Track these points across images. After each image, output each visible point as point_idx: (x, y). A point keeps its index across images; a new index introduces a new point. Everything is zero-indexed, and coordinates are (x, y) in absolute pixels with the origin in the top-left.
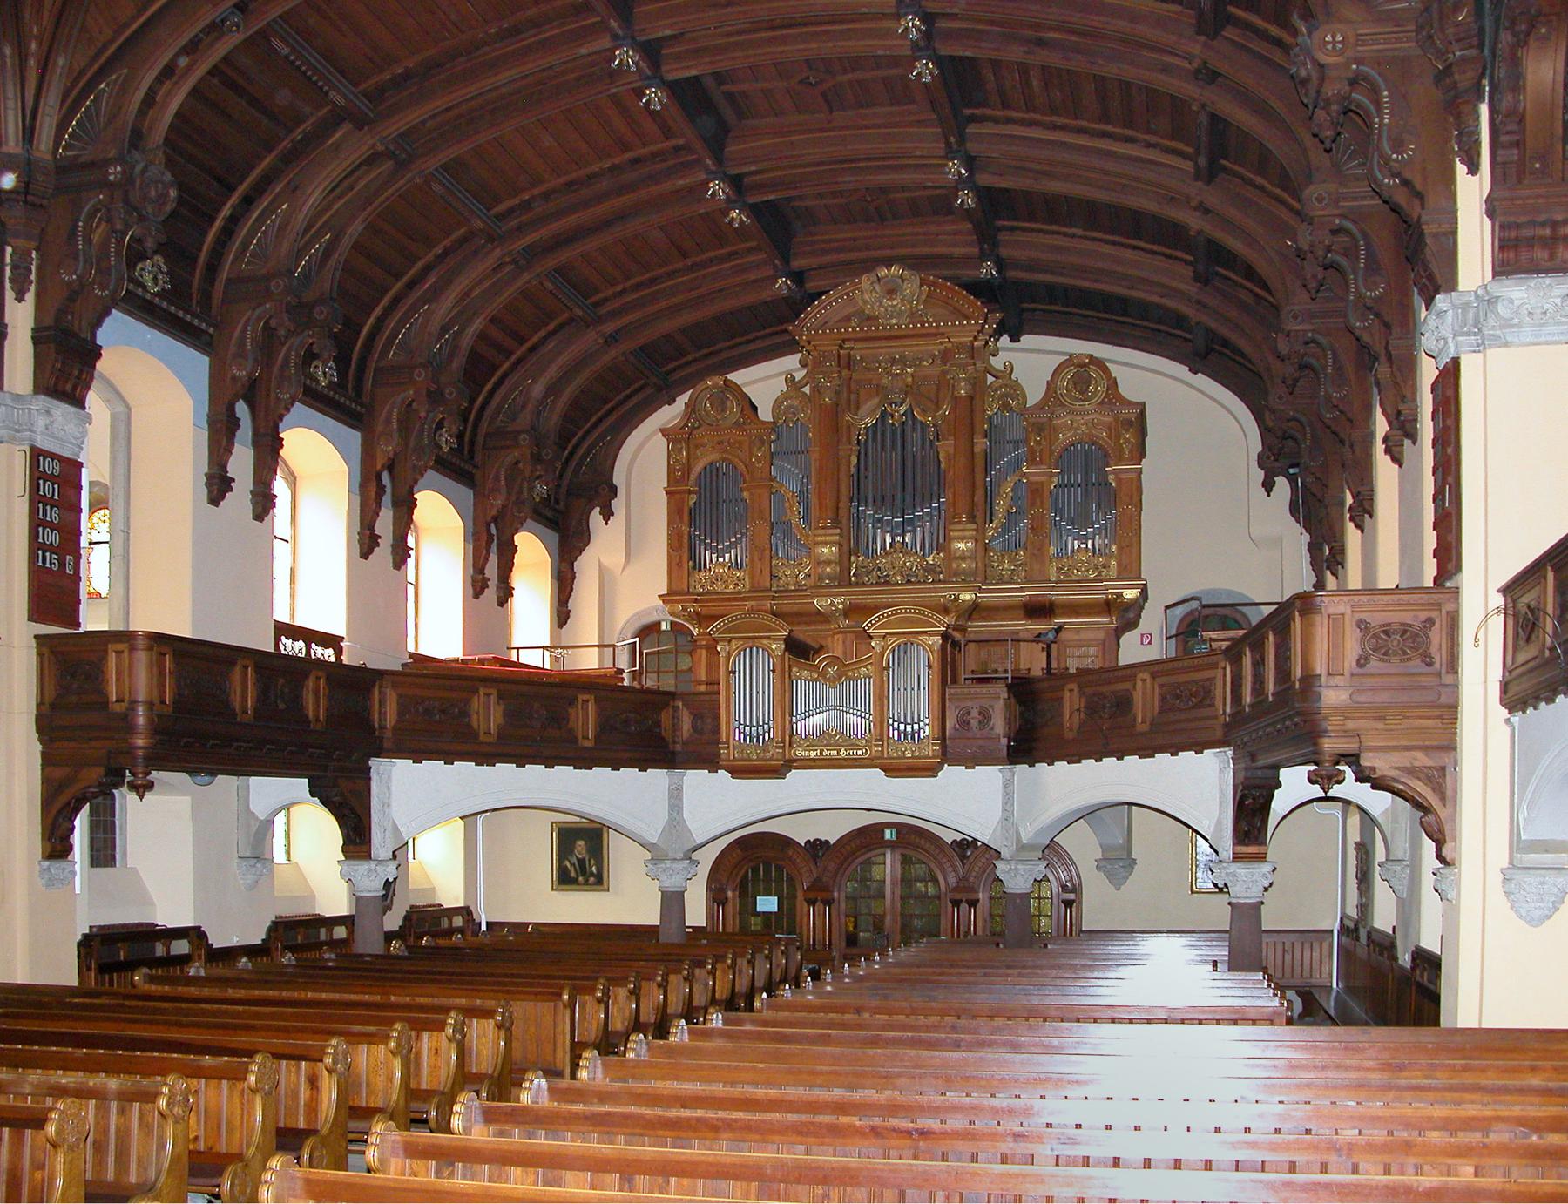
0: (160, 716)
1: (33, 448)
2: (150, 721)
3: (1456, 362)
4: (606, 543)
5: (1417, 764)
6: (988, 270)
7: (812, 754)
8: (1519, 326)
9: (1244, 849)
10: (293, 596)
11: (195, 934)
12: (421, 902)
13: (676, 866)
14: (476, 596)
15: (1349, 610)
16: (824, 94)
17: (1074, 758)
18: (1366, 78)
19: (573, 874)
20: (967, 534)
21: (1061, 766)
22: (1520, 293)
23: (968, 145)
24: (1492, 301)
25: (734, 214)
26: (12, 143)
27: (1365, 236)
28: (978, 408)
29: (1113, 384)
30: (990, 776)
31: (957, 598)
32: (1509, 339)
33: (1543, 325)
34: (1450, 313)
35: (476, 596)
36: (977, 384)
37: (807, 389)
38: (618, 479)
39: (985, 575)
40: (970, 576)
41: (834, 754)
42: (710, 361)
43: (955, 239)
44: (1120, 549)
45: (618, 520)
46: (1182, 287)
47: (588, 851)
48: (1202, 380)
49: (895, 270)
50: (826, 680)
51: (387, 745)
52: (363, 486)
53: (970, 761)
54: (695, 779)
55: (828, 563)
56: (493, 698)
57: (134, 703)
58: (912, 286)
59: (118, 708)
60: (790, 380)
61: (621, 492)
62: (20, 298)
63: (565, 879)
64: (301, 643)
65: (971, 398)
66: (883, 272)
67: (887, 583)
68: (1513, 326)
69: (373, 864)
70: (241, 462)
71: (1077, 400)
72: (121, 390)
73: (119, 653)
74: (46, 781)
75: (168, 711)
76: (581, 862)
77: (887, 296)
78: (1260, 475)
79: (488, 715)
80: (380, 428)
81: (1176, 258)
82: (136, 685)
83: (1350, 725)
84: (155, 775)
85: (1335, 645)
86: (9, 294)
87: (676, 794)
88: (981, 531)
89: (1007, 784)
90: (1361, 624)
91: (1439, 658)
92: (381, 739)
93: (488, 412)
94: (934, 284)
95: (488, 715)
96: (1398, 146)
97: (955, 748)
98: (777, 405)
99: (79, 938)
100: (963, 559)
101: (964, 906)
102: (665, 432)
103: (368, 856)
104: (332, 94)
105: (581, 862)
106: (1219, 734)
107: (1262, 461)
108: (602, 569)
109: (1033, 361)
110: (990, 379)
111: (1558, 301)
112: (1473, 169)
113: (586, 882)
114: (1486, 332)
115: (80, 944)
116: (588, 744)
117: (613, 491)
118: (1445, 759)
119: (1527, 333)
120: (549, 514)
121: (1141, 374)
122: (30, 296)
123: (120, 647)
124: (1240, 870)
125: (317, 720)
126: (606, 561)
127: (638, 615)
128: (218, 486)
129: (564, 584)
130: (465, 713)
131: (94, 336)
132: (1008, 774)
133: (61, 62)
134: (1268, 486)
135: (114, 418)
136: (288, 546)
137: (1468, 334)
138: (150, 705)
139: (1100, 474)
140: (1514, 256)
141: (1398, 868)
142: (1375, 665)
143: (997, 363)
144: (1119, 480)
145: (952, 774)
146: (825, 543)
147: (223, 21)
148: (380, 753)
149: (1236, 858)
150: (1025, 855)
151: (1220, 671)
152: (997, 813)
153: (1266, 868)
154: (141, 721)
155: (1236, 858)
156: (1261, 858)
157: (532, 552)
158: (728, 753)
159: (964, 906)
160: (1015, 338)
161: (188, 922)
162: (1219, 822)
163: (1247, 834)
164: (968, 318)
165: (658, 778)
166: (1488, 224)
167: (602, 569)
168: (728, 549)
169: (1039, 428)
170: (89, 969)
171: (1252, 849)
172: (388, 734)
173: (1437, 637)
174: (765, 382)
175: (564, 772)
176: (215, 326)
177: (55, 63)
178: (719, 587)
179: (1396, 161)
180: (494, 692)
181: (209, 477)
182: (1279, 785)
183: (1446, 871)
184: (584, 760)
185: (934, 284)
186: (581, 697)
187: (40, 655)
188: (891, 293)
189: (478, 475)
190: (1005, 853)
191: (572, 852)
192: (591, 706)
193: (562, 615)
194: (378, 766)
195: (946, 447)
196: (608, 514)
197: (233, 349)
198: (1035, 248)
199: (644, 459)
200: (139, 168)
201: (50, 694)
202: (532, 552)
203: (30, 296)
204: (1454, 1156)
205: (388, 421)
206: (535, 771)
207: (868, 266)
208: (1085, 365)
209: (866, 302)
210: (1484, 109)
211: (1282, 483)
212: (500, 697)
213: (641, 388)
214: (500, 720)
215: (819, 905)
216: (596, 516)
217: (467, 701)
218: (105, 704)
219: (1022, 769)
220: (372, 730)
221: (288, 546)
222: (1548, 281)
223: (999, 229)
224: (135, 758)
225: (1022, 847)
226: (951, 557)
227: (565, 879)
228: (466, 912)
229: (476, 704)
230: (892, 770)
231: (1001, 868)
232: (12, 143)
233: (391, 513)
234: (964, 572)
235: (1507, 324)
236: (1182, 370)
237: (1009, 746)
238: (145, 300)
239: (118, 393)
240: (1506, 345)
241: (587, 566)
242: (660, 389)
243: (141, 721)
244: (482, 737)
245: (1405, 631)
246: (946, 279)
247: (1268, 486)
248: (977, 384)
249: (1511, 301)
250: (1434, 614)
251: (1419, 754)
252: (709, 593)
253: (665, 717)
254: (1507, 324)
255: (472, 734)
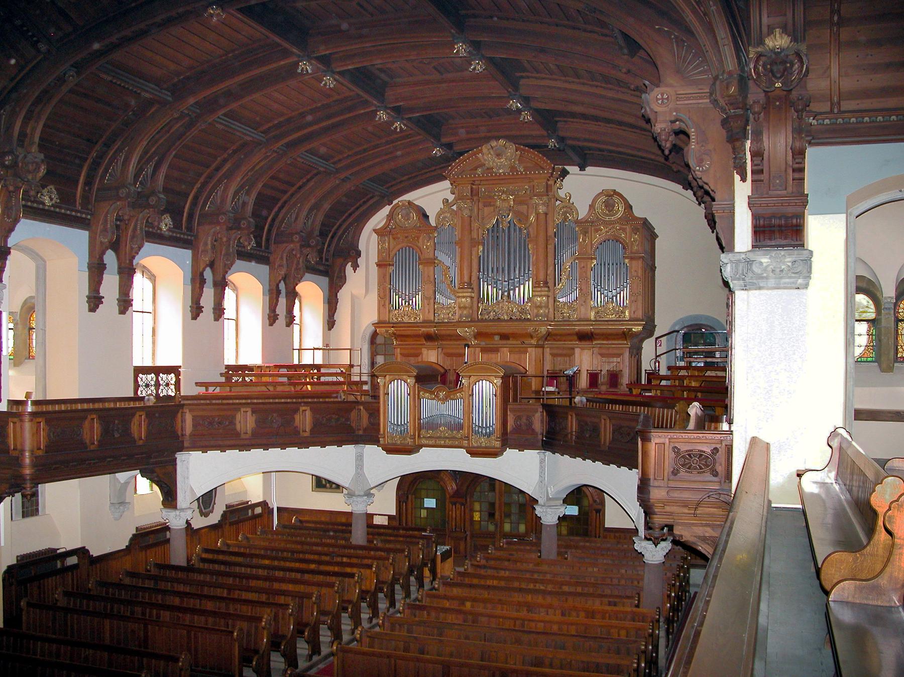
0: (36, 457)
2: (32, 461)
5: (707, 535)
6: (552, 143)
8: (767, 278)
10: (154, 343)
11: (82, 552)
12: (233, 501)
13: (359, 499)
14: (271, 325)
15: (667, 441)
16: (434, 67)
17: (573, 456)
20: (543, 293)
22: (765, 259)
23: (521, 91)
25: (397, 124)
32: (761, 285)
33: (781, 278)
34: (729, 265)
35: (271, 325)
37: (454, 208)
45: (361, 270)
49: (502, 142)
50: (440, 400)
51: (186, 444)
52: (193, 280)
53: (522, 446)
56: (249, 413)
57: (22, 451)
58: (511, 150)
59: (15, 454)
60: (446, 201)
61: (363, 254)
64: (153, 375)
66: (494, 143)
68: (763, 278)
69: (178, 512)
70: (110, 284)
71: (607, 215)
72: (41, 254)
73: (14, 423)
75: (40, 453)
77: (498, 156)
87: (360, 458)
90: (676, 450)
91: (720, 469)
92: (183, 442)
93: (277, 223)
94: (523, 150)
97: (513, 437)
98: (438, 215)
99: (4, 568)
102: (375, 231)
104: (143, 94)
111: (790, 264)
115: (5, 572)
116: (306, 434)
117: (359, 254)
119: (772, 282)
120: (321, 268)
123: (15, 420)
125: (140, 438)
126: (355, 292)
128: (95, 301)
129: (332, 304)
130: (232, 423)
131: (6, 242)
135: (38, 268)
136: (150, 316)
137: (739, 279)
138: (32, 452)
142: (683, 473)
145: (511, 454)
147: (65, 74)
148: (181, 449)
150: (552, 503)
152: (537, 478)
154: (27, 461)
157: (311, 291)
160: (582, 168)
161: (78, 545)
162: (639, 514)
164: (543, 168)
165: (349, 450)
167: (353, 298)
170: (11, 584)
172: (187, 437)
173: (721, 456)
174: (433, 198)
175: (292, 451)
176: (91, 215)
178: (406, 319)
179: (699, 171)
180: (249, 410)
184: (304, 444)
185: (523, 150)
186: (302, 408)
188: (498, 155)
189: (271, 258)
192: (308, 413)
193: (330, 323)
194: (180, 457)
196: (355, 266)
199: (369, 242)
200: (20, 158)
202: (311, 291)
205: (206, 244)
206: (275, 452)
207: (487, 139)
208: (612, 196)
209: (485, 160)
212: (253, 412)
213: (371, 198)
214: (254, 425)
215: (458, 506)
216: (349, 268)
217: (234, 417)
218: (7, 451)
220: (178, 437)
221: (150, 316)
222: (783, 253)
223: (557, 122)
224: (25, 480)
225: (549, 499)
228: (264, 504)
229: (239, 417)
231: (539, 511)
233: (212, 290)
235: (760, 277)
238: (47, 210)
239: (37, 255)
240: (760, 288)
241: (344, 295)
243: (27, 461)
249: (761, 263)
250: (718, 446)
251: (708, 529)
252: (400, 323)
253: (353, 415)
254: (760, 277)
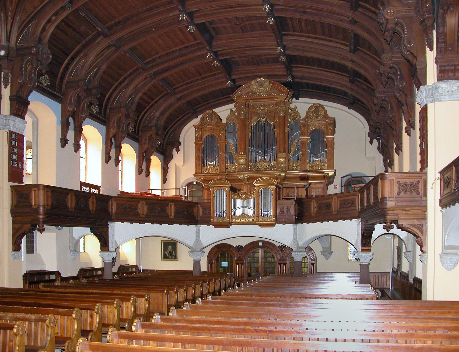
0: (47, 209)
1: (10, 131)
2: (44, 211)
3: (426, 106)
4: (177, 159)
5: (415, 223)
6: (289, 79)
7: (238, 221)
8: (445, 95)
9: (364, 248)
10: (86, 174)
11: (57, 273)
12: (123, 264)
13: (198, 253)
14: (139, 174)
15: (395, 178)
16: (241, 28)
17: (314, 222)
18: (400, 23)
19: (168, 256)
20: (283, 156)
21: (311, 224)
22: (445, 86)
23: (283, 42)
24: (437, 88)
25: (215, 63)
26: (3, 42)
27: (400, 69)
28: (286, 119)
29: (326, 112)
30: (290, 227)
31: (280, 175)
32: (442, 99)
33: (452, 95)
34: (425, 91)
35: (139, 174)
36: (286, 112)
37: (236, 114)
38: (181, 140)
39: (288, 168)
40: (284, 168)
41: (244, 221)
42: (208, 106)
43: (279, 70)
44: (328, 160)
45: (181, 152)
46: (346, 84)
47: (172, 249)
48: (352, 111)
49: (262, 79)
50: (242, 199)
51: (113, 218)
52: (106, 142)
53: (284, 223)
54: (203, 228)
55: (242, 164)
56: (144, 204)
57: (39, 205)
58: (267, 84)
59: (35, 207)
60: (231, 111)
61: (182, 144)
62: (6, 87)
63: (165, 257)
64: (88, 188)
65: (284, 116)
66: (258, 80)
67: (260, 170)
68: (443, 95)
69: (109, 253)
70: (71, 135)
71: (315, 117)
72: (36, 114)
73: (35, 191)
74: (13, 228)
75: (49, 208)
76: (170, 252)
77: (260, 86)
78: (369, 139)
79: (143, 209)
80: (111, 125)
81: (344, 76)
82: (40, 200)
83: (395, 212)
84: (45, 227)
85: (391, 189)
86: (3, 86)
87: (198, 232)
88: (287, 155)
89: (295, 229)
90: (398, 183)
91: (421, 192)
92: (112, 216)
93: (143, 120)
94: (273, 83)
95: (143, 209)
96: (409, 43)
97: (280, 219)
98: (227, 118)
99: (23, 274)
100: (282, 163)
101: (282, 265)
102: (195, 126)
103: (108, 250)
104: (97, 27)
105: (170, 252)
106: (357, 215)
107: (369, 135)
108: (176, 166)
109: (302, 105)
110: (290, 111)
111: (456, 88)
112: (431, 49)
113: (172, 258)
114: (435, 97)
115: (23, 276)
116: (172, 217)
117: (180, 144)
118: (423, 222)
119: (447, 97)
120: (161, 150)
121: (334, 109)
122: (9, 87)
123: (35, 189)
124: (363, 254)
125: (93, 210)
126: (177, 164)
127: (187, 180)
128: (64, 142)
129: (165, 171)
130: (136, 209)
131: (27, 98)
132: (295, 226)
133: (18, 18)
134: (371, 142)
135: (33, 122)
136: (84, 160)
137: (430, 98)
138: (44, 206)
139: (322, 139)
140: (443, 75)
141: (409, 254)
142: (402, 194)
143: (292, 106)
144: (327, 140)
145: (279, 226)
146: (242, 159)
147: (65, 6)
148: (111, 220)
149: (362, 251)
150: (300, 250)
151: (357, 196)
152: (292, 238)
153: (370, 254)
154: (41, 211)
155: (362, 251)
156: (369, 251)
157: (156, 161)
158: (213, 220)
159: (282, 265)
160: (297, 99)
161: (55, 270)
162: (357, 240)
163: (365, 244)
164: (283, 93)
165: (193, 227)
166: (435, 65)
167: (176, 166)
168: (213, 161)
169: (304, 125)
170: (26, 283)
171: (366, 248)
172: (114, 215)
173: (421, 186)
174: (224, 112)
175: (165, 226)
176: (63, 95)
177: (16, 18)
178: (210, 172)
179: (409, 47)
180: (145, 202)
181: (61, 139)
182: (374, 230)
183: (423, 255)
184: (171, 222)
185: (273, 83)
186: (170, 204)
187: (12, 191)
188: (261, 86)
189: (140, 139)
190: (294, 249)
191: (167, 249)
192: (173, 206)
193: (164, 180)
194: (111, 224)
195: (277, 131)
196: (178, 150)
197: (68, 102)
198: (303, 73)
199: (189, 134)
200: (41, 49)
201: (15, 203)
202: (156, 161)
203: (9, 87)
204: (426, 338)
205: (114, 123)
206: (157, 225)
207: (254, 78)
208: (318, 107)
209: (253, 88)
210: (434, 32)
211: (375, 141)
212: (146, 204)
213: (188, 113)
214: (146, 211)
215: (240, 265)
216: (174, 151)
217: (137, 205)
218: (31, 206)
219: (299, 225)
220: (109, 213)
221: (84, 160)
222: (453, 82)
223: (293, 67)
224: (39, 221)
225: (299, 248)
226: (278, 163)
227: (165, 257)
228: (136, 267)
229: (139, 206)
230: (261, 225)
231: (293, 254)
232: (3, 42)
233: (114, 150)
234: (282, 167)
235: (441, 95)
236: (346, 108)
237: (295, 218)
238: (43, 88)
239: (35, 115)
240: (441, 101)
241: (172, 165)
242: (193, 114)
243: (41, 211)
244: (141, 216)
245: (411, 185)
246: (277, 82)
247: (371, 142)
248: (286, 112)
249: (442, 88)
250: (420, 180)
251: (415, 221)
252: (207, 173)
253: (195, 210)
254: (441, 95)
255: (138, 215)
